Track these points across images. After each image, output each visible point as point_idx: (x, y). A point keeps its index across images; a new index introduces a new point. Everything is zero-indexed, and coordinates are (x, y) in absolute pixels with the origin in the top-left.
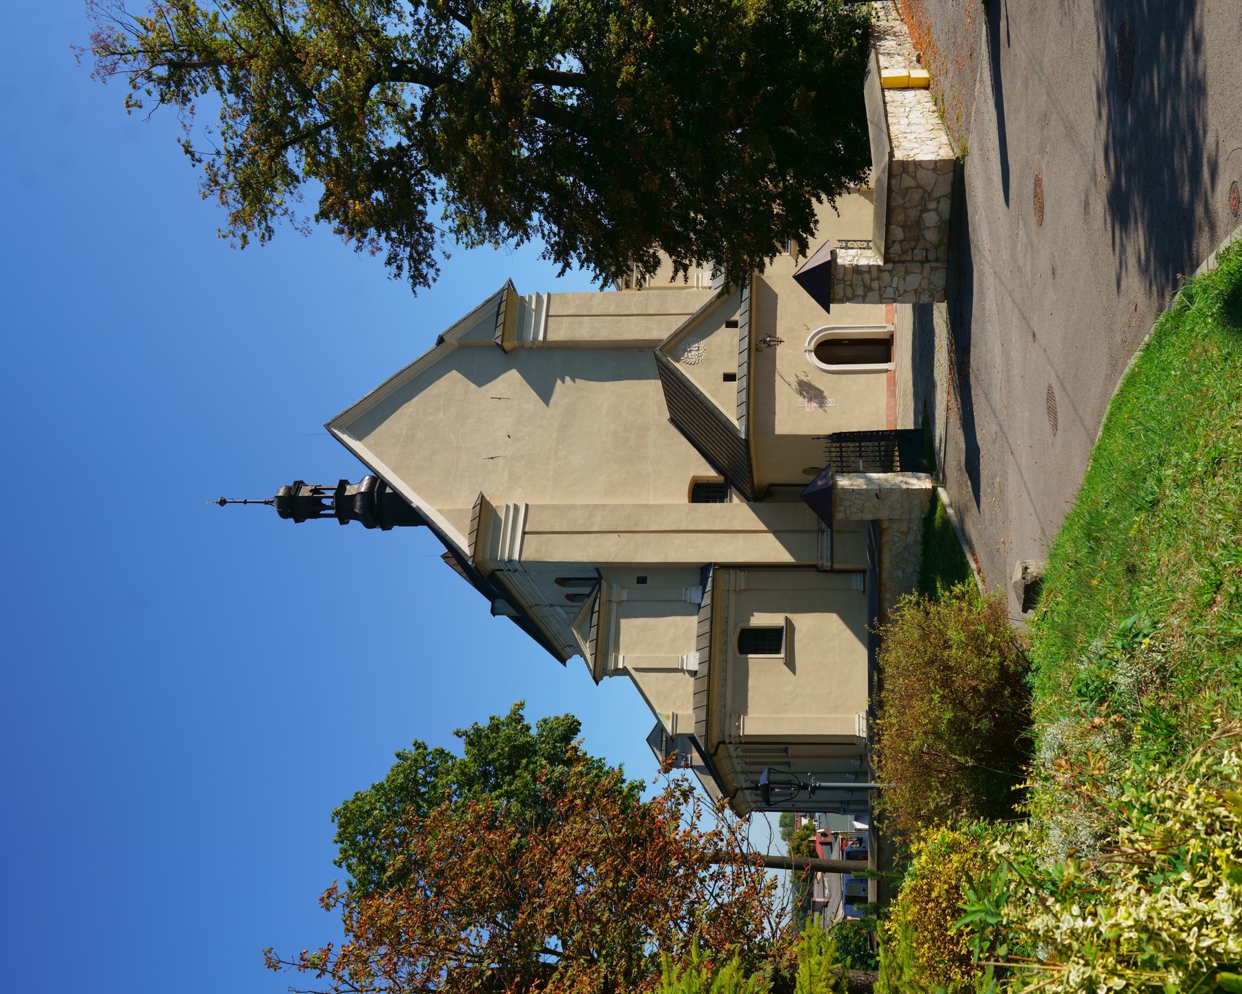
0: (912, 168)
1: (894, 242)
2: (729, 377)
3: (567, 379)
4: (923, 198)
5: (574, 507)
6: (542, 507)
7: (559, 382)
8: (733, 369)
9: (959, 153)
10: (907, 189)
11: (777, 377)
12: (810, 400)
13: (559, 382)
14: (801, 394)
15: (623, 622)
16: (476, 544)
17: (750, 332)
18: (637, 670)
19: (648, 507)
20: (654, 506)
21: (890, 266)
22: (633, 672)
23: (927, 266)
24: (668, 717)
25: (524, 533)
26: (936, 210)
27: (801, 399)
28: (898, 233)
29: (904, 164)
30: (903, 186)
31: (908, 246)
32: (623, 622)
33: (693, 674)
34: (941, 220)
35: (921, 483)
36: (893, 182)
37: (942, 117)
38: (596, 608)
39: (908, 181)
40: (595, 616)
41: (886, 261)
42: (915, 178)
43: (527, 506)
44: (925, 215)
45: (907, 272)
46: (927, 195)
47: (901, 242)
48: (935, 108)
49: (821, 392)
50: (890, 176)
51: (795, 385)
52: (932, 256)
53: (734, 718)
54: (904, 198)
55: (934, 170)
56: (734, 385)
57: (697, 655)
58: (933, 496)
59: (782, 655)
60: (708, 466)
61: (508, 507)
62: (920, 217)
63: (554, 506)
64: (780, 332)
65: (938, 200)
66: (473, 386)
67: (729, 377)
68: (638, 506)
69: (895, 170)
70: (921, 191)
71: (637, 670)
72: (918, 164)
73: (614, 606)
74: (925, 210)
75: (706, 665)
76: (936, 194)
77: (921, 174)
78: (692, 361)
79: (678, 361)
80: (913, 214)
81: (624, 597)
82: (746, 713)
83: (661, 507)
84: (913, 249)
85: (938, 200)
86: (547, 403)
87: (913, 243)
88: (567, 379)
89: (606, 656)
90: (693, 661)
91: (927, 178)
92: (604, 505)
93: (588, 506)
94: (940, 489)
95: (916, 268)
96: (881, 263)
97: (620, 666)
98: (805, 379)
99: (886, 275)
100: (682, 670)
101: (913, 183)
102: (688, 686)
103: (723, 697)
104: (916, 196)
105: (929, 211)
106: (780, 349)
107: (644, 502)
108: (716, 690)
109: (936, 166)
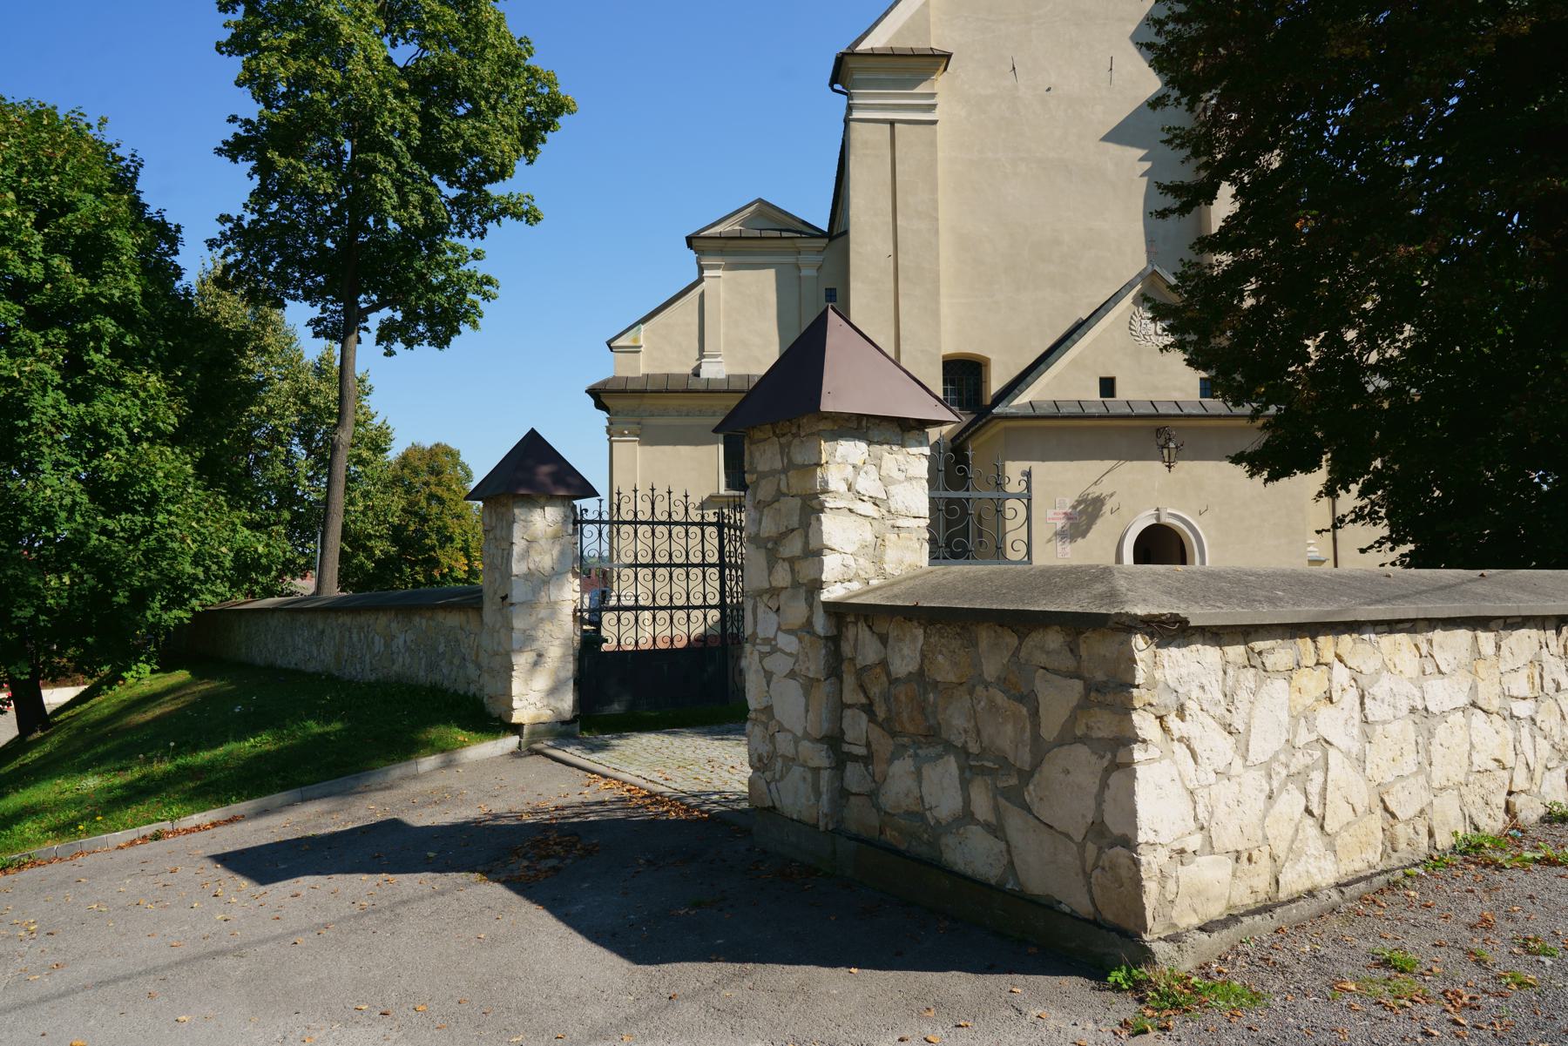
0: (1103, 725)
1: (884, 640)
2: (1108, 386)
3: (1147, 165)
4: (1004, 764)
5: (934, 189)
6: (933, 144)
7: (1141, 153)
8: (1123, 392)
9: (1172, 960)
10: (1029, 700)
11: (1109, 464)
12: (1068, 516)
13: (1141, 153)
14: (1079, 502)
15: (770, 274)
16: (872, 55)
17: (1189, 416)
18: (702, 296)
19: (935, 295)
20: (937, 302)
21: (820, 624)
22: (698, 290)
23: (819, 757)
24: (636, 340)
25: (892, 123)
26: (966, 816)
27: (1069, 502)
28: (905, 657)
29: (1114, 691)
30: (1039, 686)
31: (875, 691)
32: (770, 274)
33: (696, 374)
34: (940, 829)
35: (536, 692)
36: (1054, 639)
37: (1472, 851)
38: (785, 234)
39: (1058, 700)
40: (777, 234)
41: (838, 611)
42: (1068, 738)
43: (934, 122)
44: (951, 764)
45: (809, 686)
46: (1012, 780)
47: (884, 664)
48: (1530, 811)
49: (1084, 535)
50: (1078, 625)
51: (1096, 491)
52: (854, 776)
53: (635, 427)
54: (1003, 683)
55: (1098, 830)
56: (1094, 394)
57: (722, 376)
58: (489, 718)
59: (722, 491)
60: (1007, 379)
61: (933, 95)
62: (949, 747)
63: (934, 161)
64: (1184, 467)
65: (996, 830)
66: (1132, 28)
67: (1108, 386)
68: (936, 281)
69: (1096, 646)
70: (1024, 758)
71: (702, 296)
72: (1116, 754)
73: (791, 259)
74: (971, 767)
75: (703, 387)
76: (1015, 822)
77: (1081, 766)
78: (1137, 326)
79: (1135, 302)
80: (956, 720)
81: (805, 272)
82: (643, 443)
83: (936, 314)
84: (868, 709)
85: (996, 830)
86: (1107, 138)
87: (881, 714)
88: (1147, 165)
89: (721, 252)
90: (713, 371)
91: (1066, 786)
92: (937, 232)
93: (936, 209)
94: (512, 742)
95: (819, 724)
96: (825, 596)
97: (706, 273)
98: (1106, 509)
99: (796, 611)
100: (702, 356)
101: (1050, 731)
102: (680, 365)
103: (664, 413)
104: (1007, 736)
105: (965, 784)
106: (1159, 466)
107: (943, 290)
108: (673, 402)
109: (1113, 839)
